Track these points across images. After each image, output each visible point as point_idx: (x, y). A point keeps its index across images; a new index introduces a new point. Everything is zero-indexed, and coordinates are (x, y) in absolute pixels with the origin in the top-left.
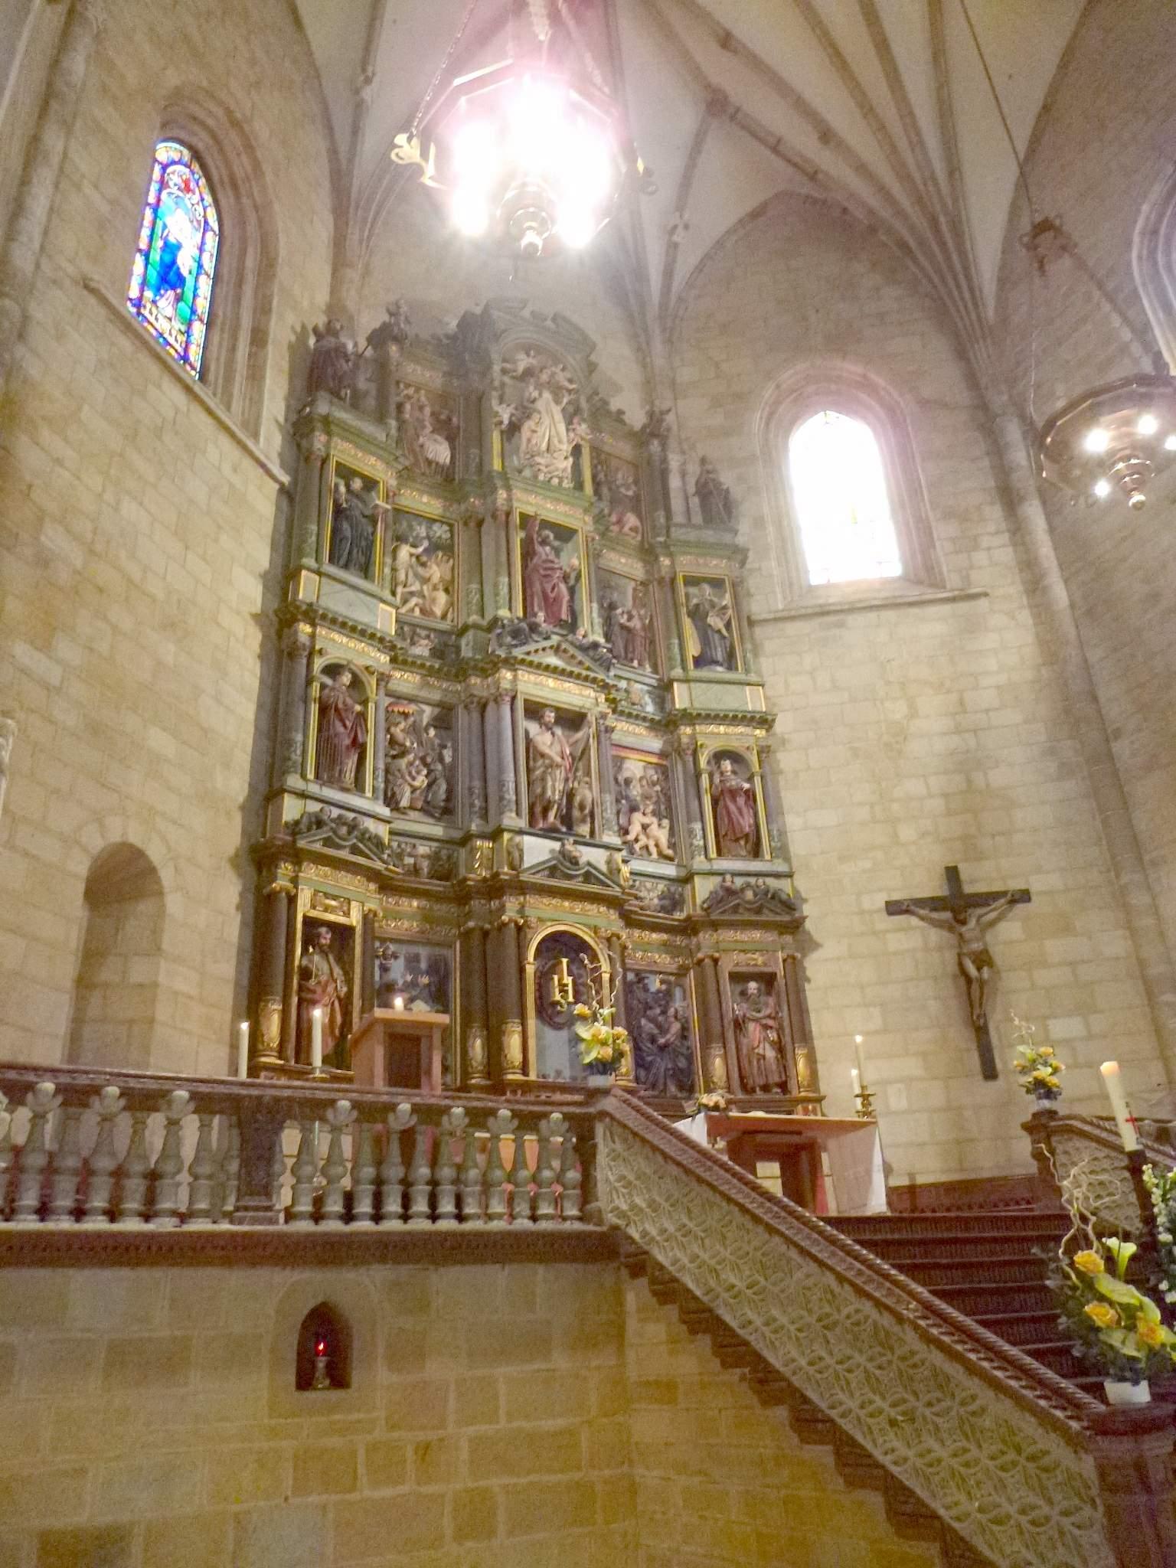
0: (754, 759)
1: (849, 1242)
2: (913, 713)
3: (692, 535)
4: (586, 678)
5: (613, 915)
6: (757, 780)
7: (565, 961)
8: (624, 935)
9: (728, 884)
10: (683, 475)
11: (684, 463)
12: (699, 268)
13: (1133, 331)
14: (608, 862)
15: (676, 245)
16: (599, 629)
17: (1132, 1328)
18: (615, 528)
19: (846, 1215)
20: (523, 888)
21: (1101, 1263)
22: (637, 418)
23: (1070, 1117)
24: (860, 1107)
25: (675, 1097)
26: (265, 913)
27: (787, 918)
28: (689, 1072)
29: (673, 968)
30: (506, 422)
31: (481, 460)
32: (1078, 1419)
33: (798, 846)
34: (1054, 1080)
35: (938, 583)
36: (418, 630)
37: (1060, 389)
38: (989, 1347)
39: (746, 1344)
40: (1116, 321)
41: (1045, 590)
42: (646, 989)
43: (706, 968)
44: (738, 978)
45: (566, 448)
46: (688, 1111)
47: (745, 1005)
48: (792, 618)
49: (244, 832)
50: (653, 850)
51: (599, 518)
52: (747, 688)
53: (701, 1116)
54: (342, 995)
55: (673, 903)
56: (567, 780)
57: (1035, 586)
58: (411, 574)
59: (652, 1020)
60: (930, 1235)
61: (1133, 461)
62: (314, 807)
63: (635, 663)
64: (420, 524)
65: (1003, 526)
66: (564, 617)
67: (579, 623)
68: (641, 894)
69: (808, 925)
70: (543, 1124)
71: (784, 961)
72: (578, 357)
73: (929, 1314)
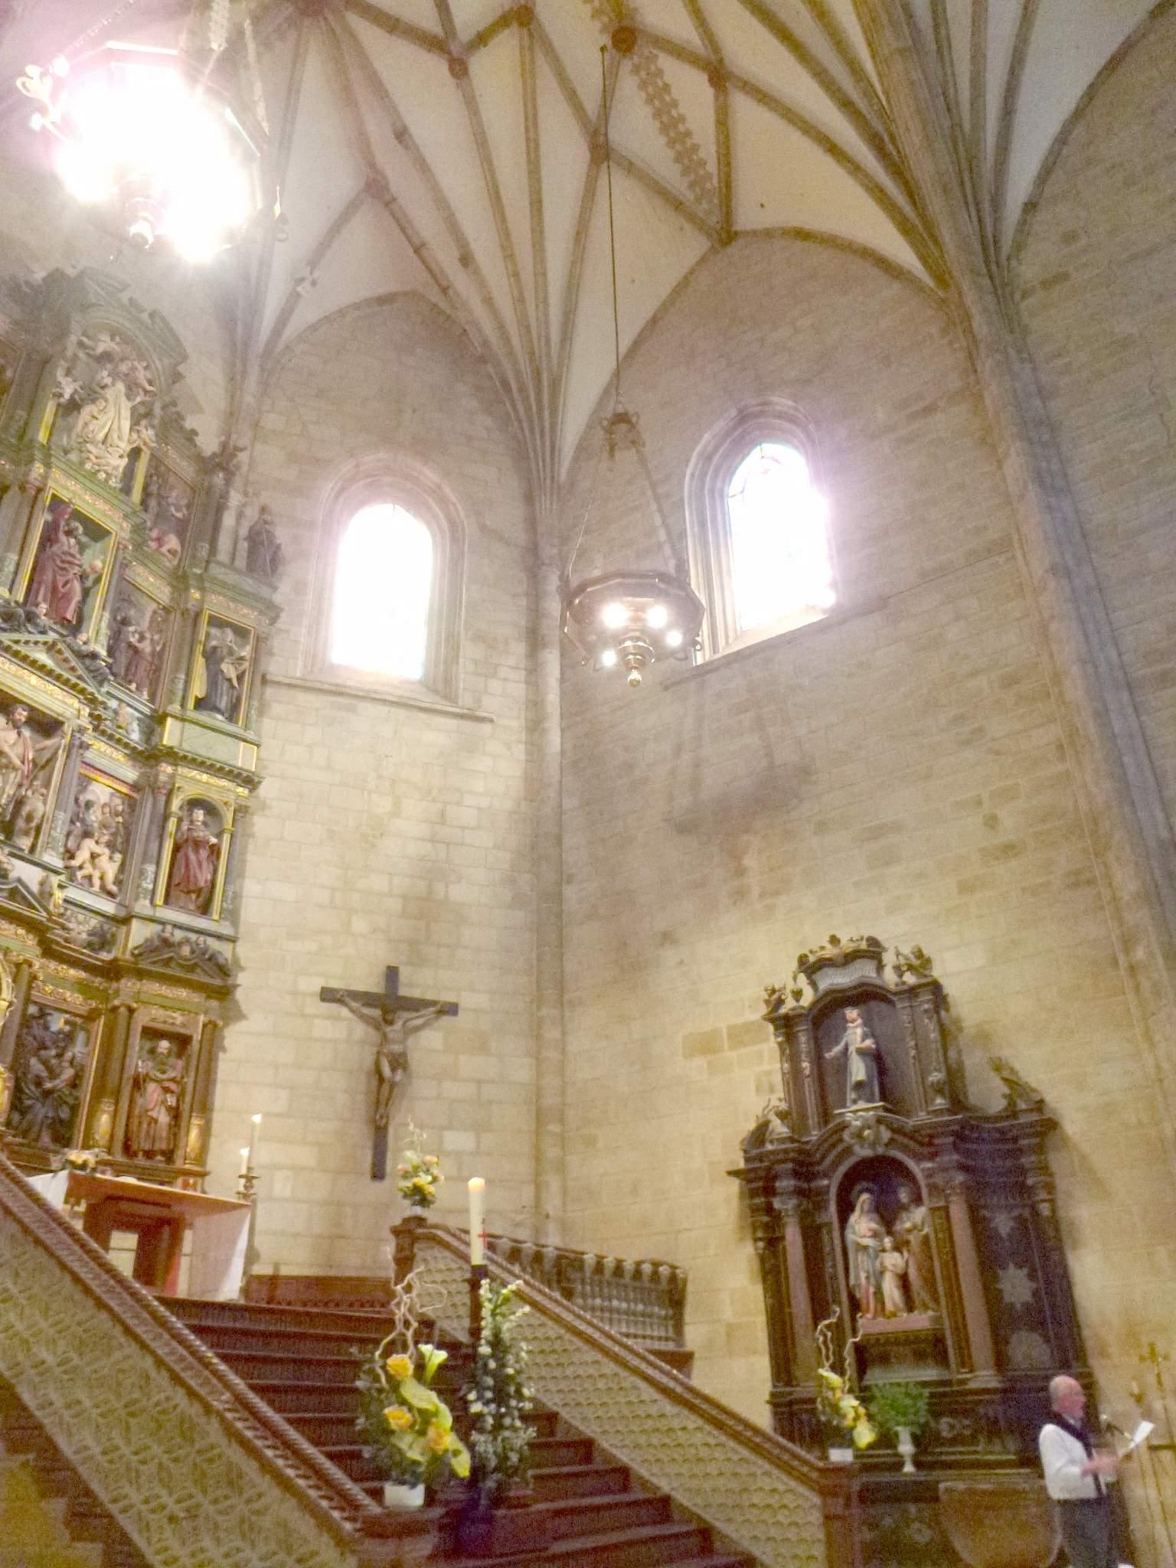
0: (229, 817)
1: (179, 1325)
2: (396, 813)
3: (231, 578)
4: (74, 687)
5: (31, 941)
6: (226, 837)
8: (37, 964)
9: (167, 935)
10: (240, 515)
11: (244, 505)
12: (313, 328)
13: (669, 534)
14: (42, 884)
15: (299, 295)
16: (103, 639)
17: (422, 1433)
18: (153, 545)
19: (195, 1298)
21: (411, 1367)
22: (209, 444)
23: (436, 1227)
24: (242, 1189)
25: (47, 1150)
27: (218, 982)
28: (70, 1124)
29: (83, 1010)
30: (67, 396)
31: (26, 424)
32: (353, 1520)
33: (250, 912)
34: (431, 1189)
35: (450, 697)
37: (599, 561)
38: (287, 1445)
39: (39, 1427)
40: (658, 520)
41: (544, 731)
42: (46, 1028)
43: (118, 1019)
44: (152, 1034)
45: (125, 447)
46: (54, 1167)
47: (150, 1064)
50: (97, 882)
51: (138, 529)
52: (242, 744)
53: (64, 1174)
55: (102, 941)
56: (20, 786)
57: (535, 726)
59: (45, 1063)
60: (272, 1328)
61: (640, 644)
63: (133, 686)
65: (523, 664)
66: (69, 616)
67: (85, 624)
68: (70, 926)
69: (239, 995)
71: (205, 1026)
72: (166, 361)
73: (239, 1407)
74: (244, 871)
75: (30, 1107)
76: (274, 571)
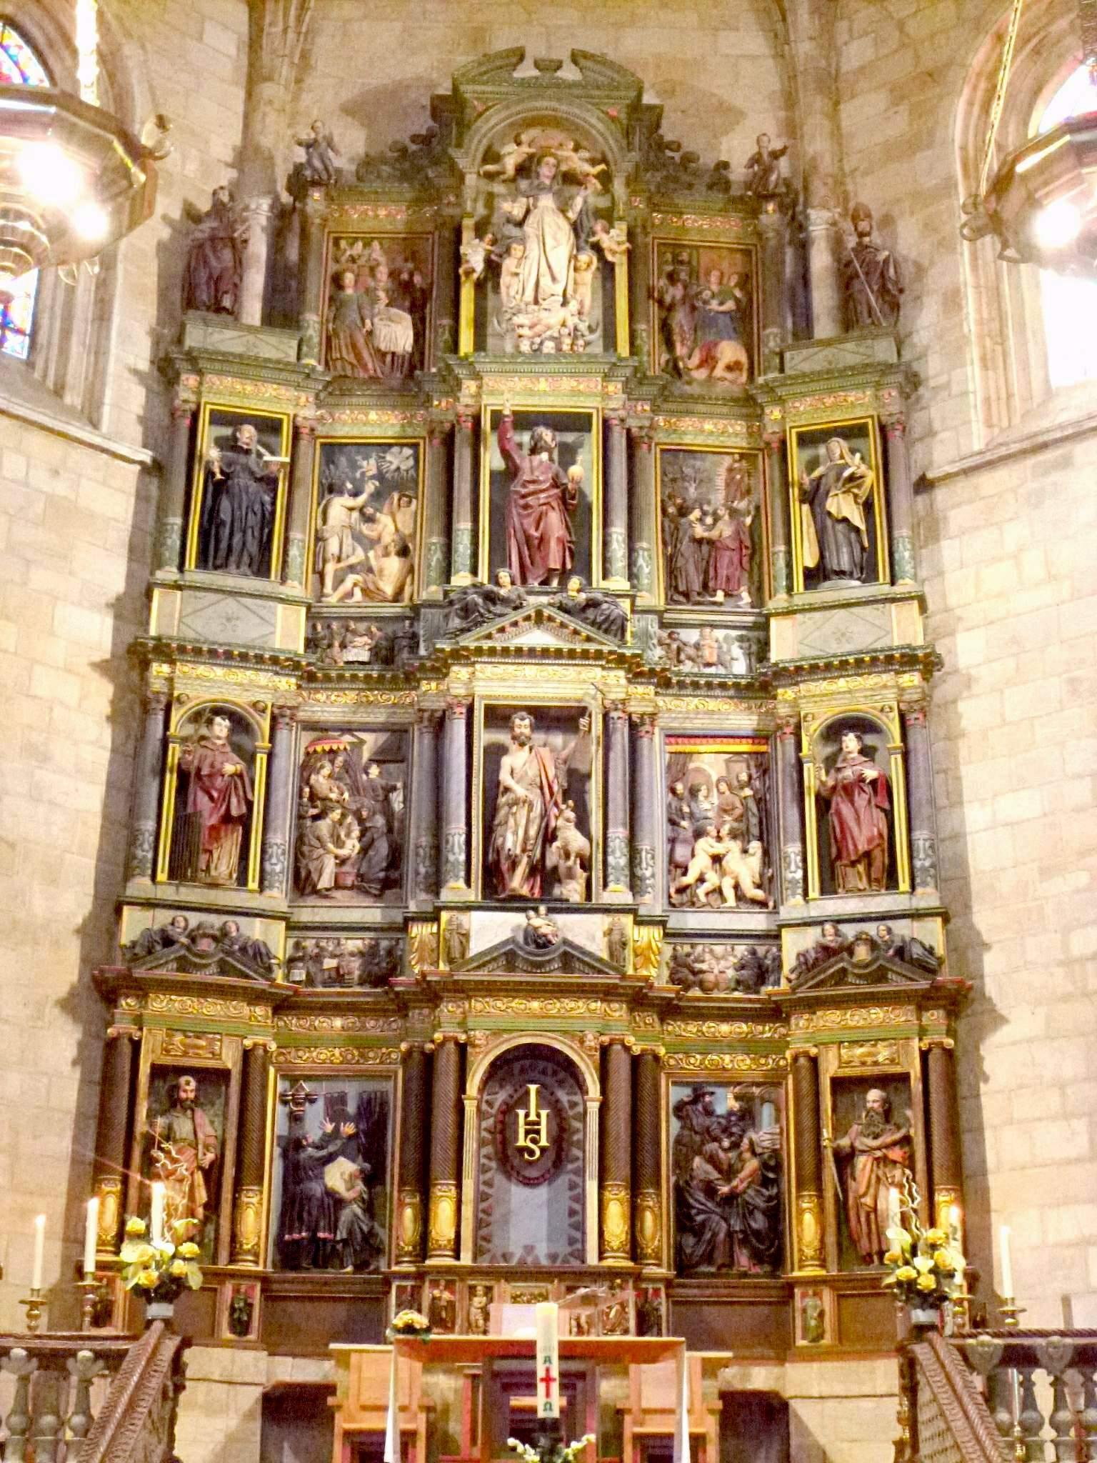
7: (533, 1088)
20: (463, 991)
26: (110, 1066)
36: (352, 625)
42: (709, 1112)
48: (990, 464)
49: (85, 960)
50: (729, 893)
54: (206, 1164)
55: (760, 972)
58: (348, 541)
59: (712, 1160)
62: (162, 918)
63: (720, 596)
64: (366, 458)
70: (70, 1363)
74: (960, 795)
75: (703, 1224)
76: (895, 307)
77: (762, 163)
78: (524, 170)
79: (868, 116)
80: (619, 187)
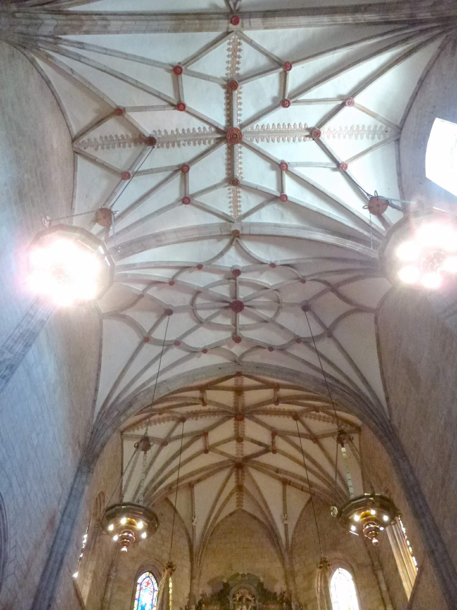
77: (282, 594)
78: (241, 599)
79: (299, 579)
80: (257, 601)
